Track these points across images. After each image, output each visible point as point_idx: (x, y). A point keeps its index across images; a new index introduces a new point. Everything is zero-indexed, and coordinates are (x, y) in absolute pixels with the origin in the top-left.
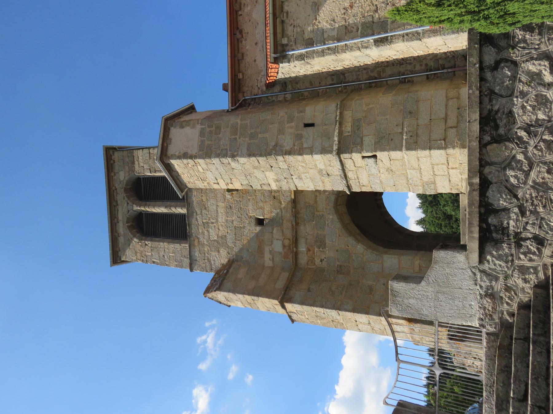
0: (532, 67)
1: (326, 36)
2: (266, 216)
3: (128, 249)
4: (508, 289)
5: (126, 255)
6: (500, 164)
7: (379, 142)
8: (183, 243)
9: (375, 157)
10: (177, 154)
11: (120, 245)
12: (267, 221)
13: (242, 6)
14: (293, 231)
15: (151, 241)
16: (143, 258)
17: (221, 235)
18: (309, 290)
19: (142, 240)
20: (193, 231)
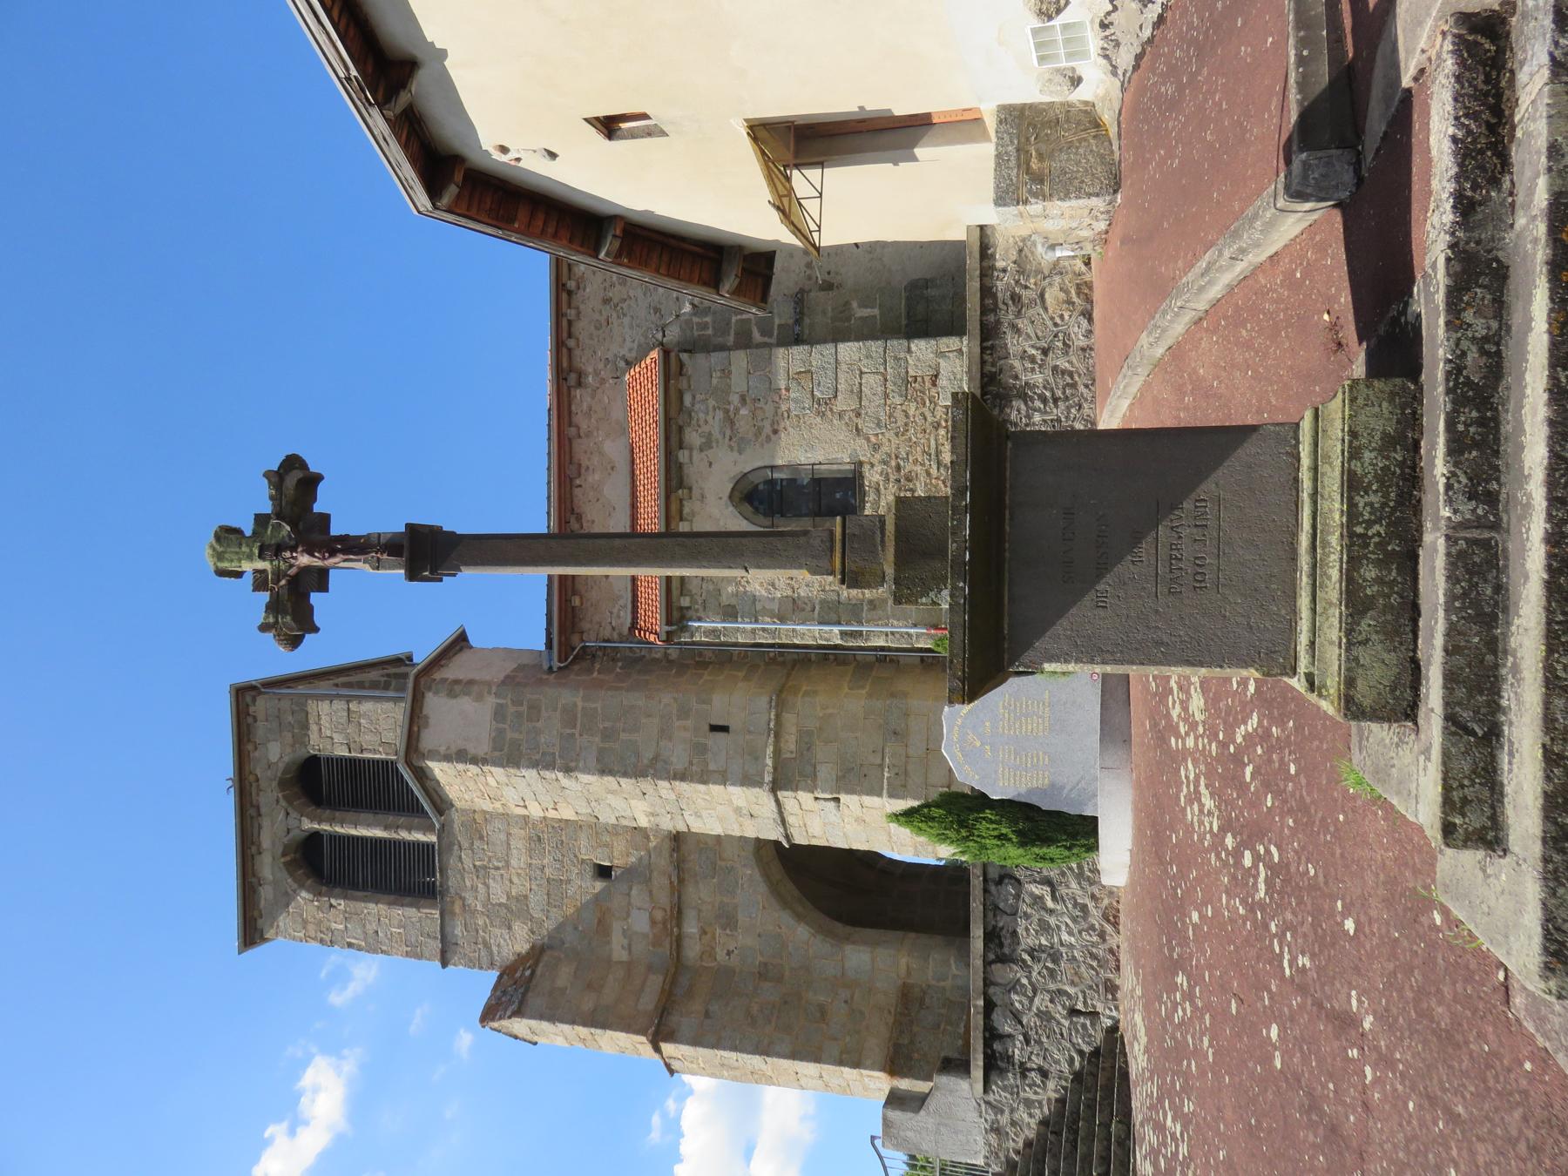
0: (1036, 889)
1: (759, 607)
2: (616, 862)
3: (284, 914)
4: (1013, 1123)
5: (278, 926)
6: (1005, 985)
7: (844, 776)
8: (425, 907)
9: (837, 800)
10: (442, 749)
11: (262, 903)
12: (619, 872)
13: (583, 471)
14: (672, 894)
15: (345, 898)
16: (322, 935)
17: (517, 893)
18: (707, 1015)
19: (320, 894)
20: (450, 884)
